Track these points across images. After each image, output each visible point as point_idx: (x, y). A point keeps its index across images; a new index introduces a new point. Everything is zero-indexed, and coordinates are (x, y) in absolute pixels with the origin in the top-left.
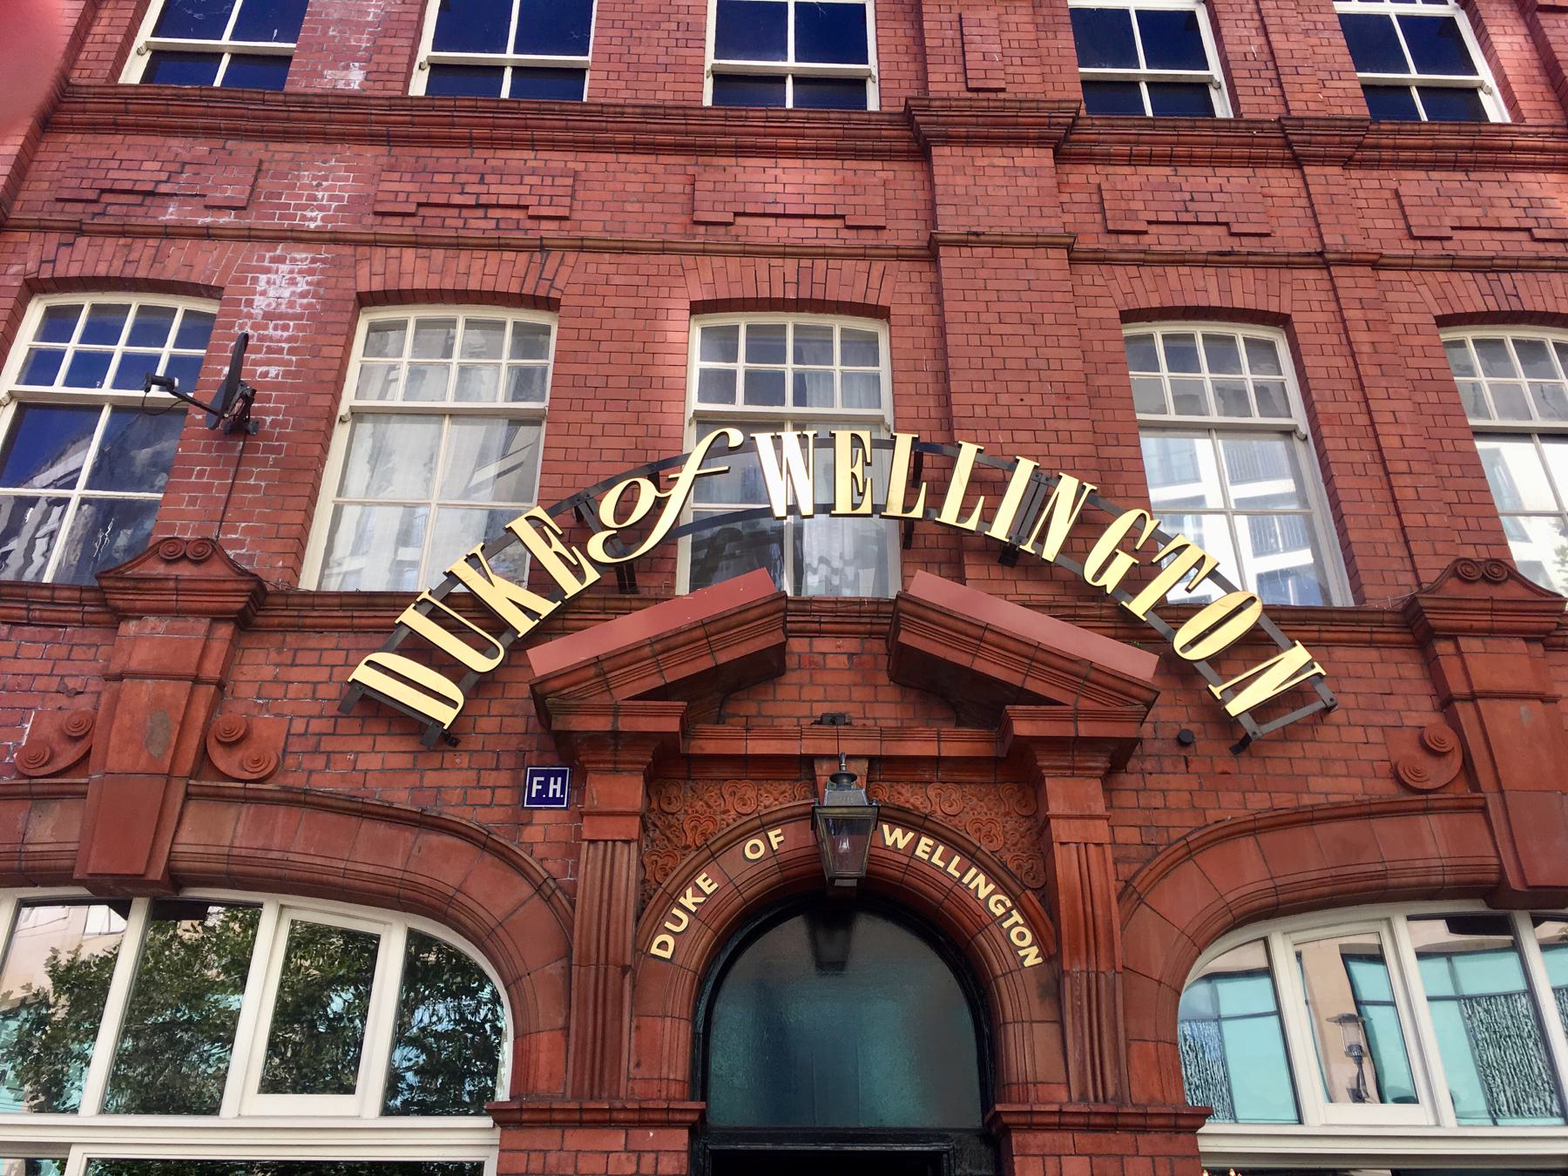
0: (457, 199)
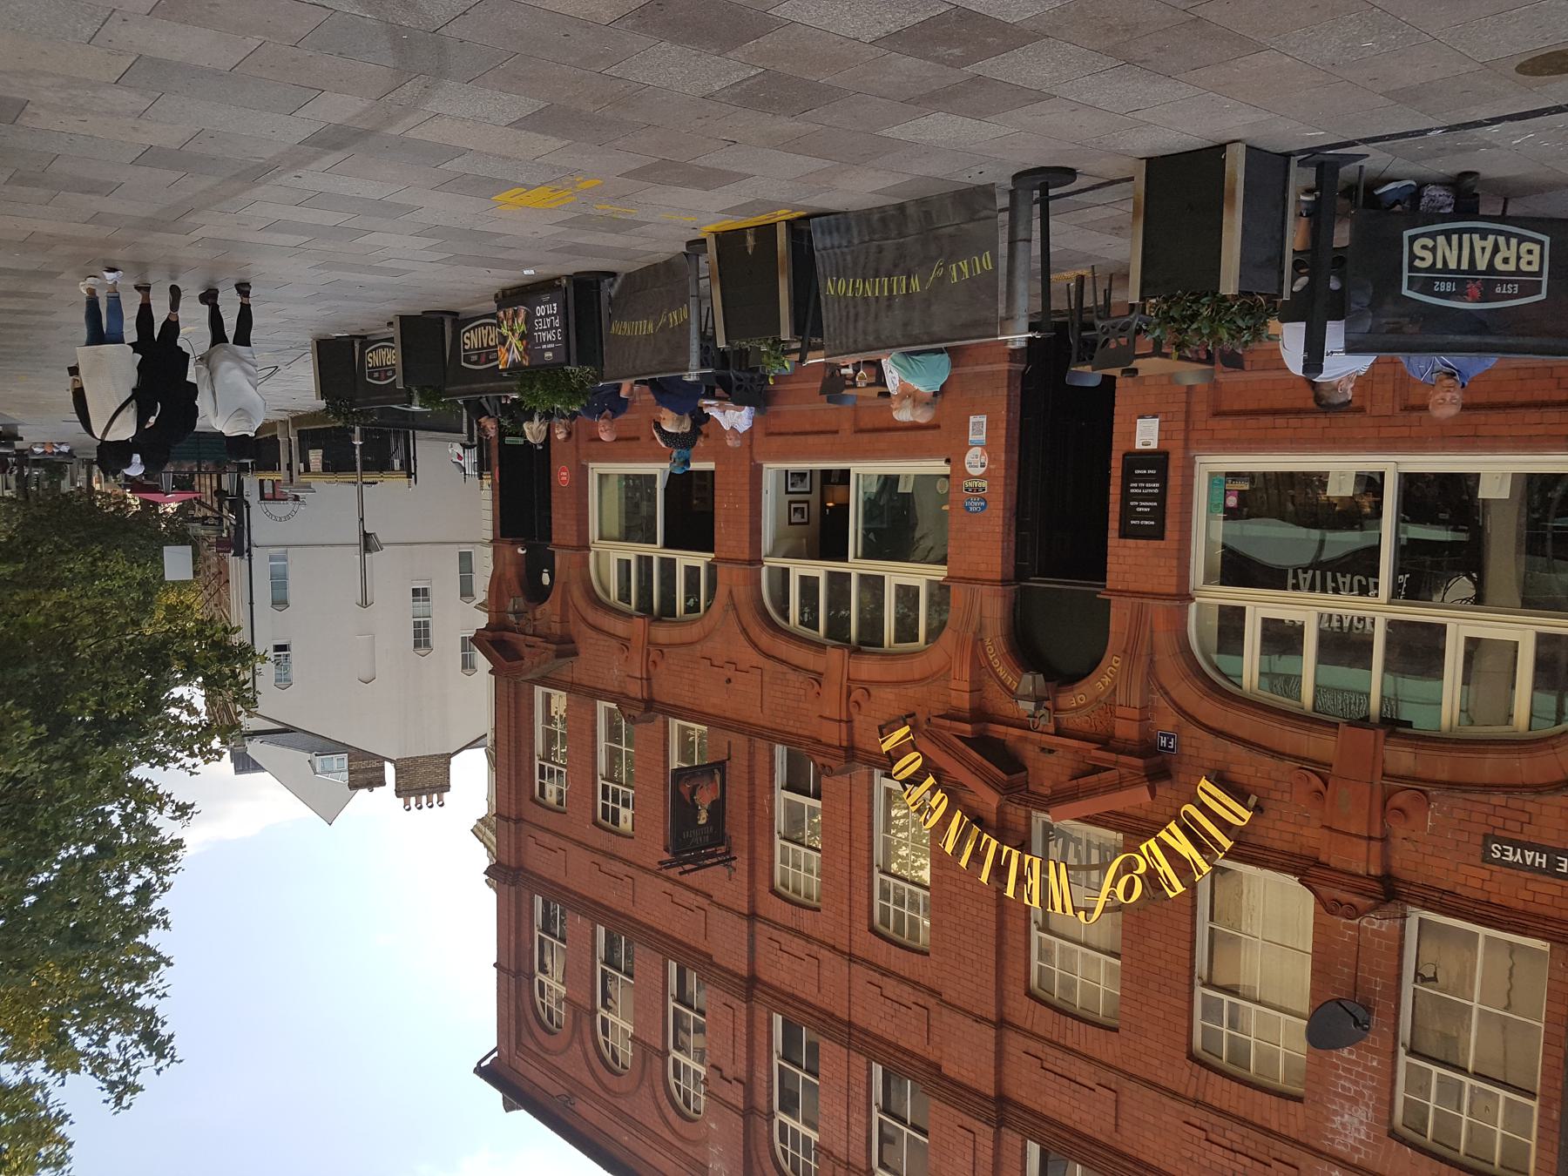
0: (1247, 1161)
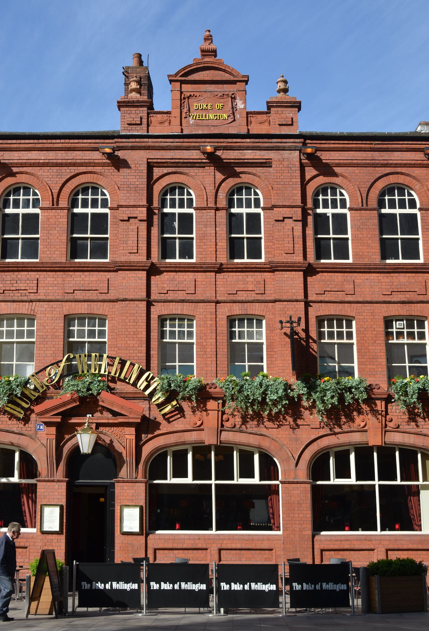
0: (12, 289)
